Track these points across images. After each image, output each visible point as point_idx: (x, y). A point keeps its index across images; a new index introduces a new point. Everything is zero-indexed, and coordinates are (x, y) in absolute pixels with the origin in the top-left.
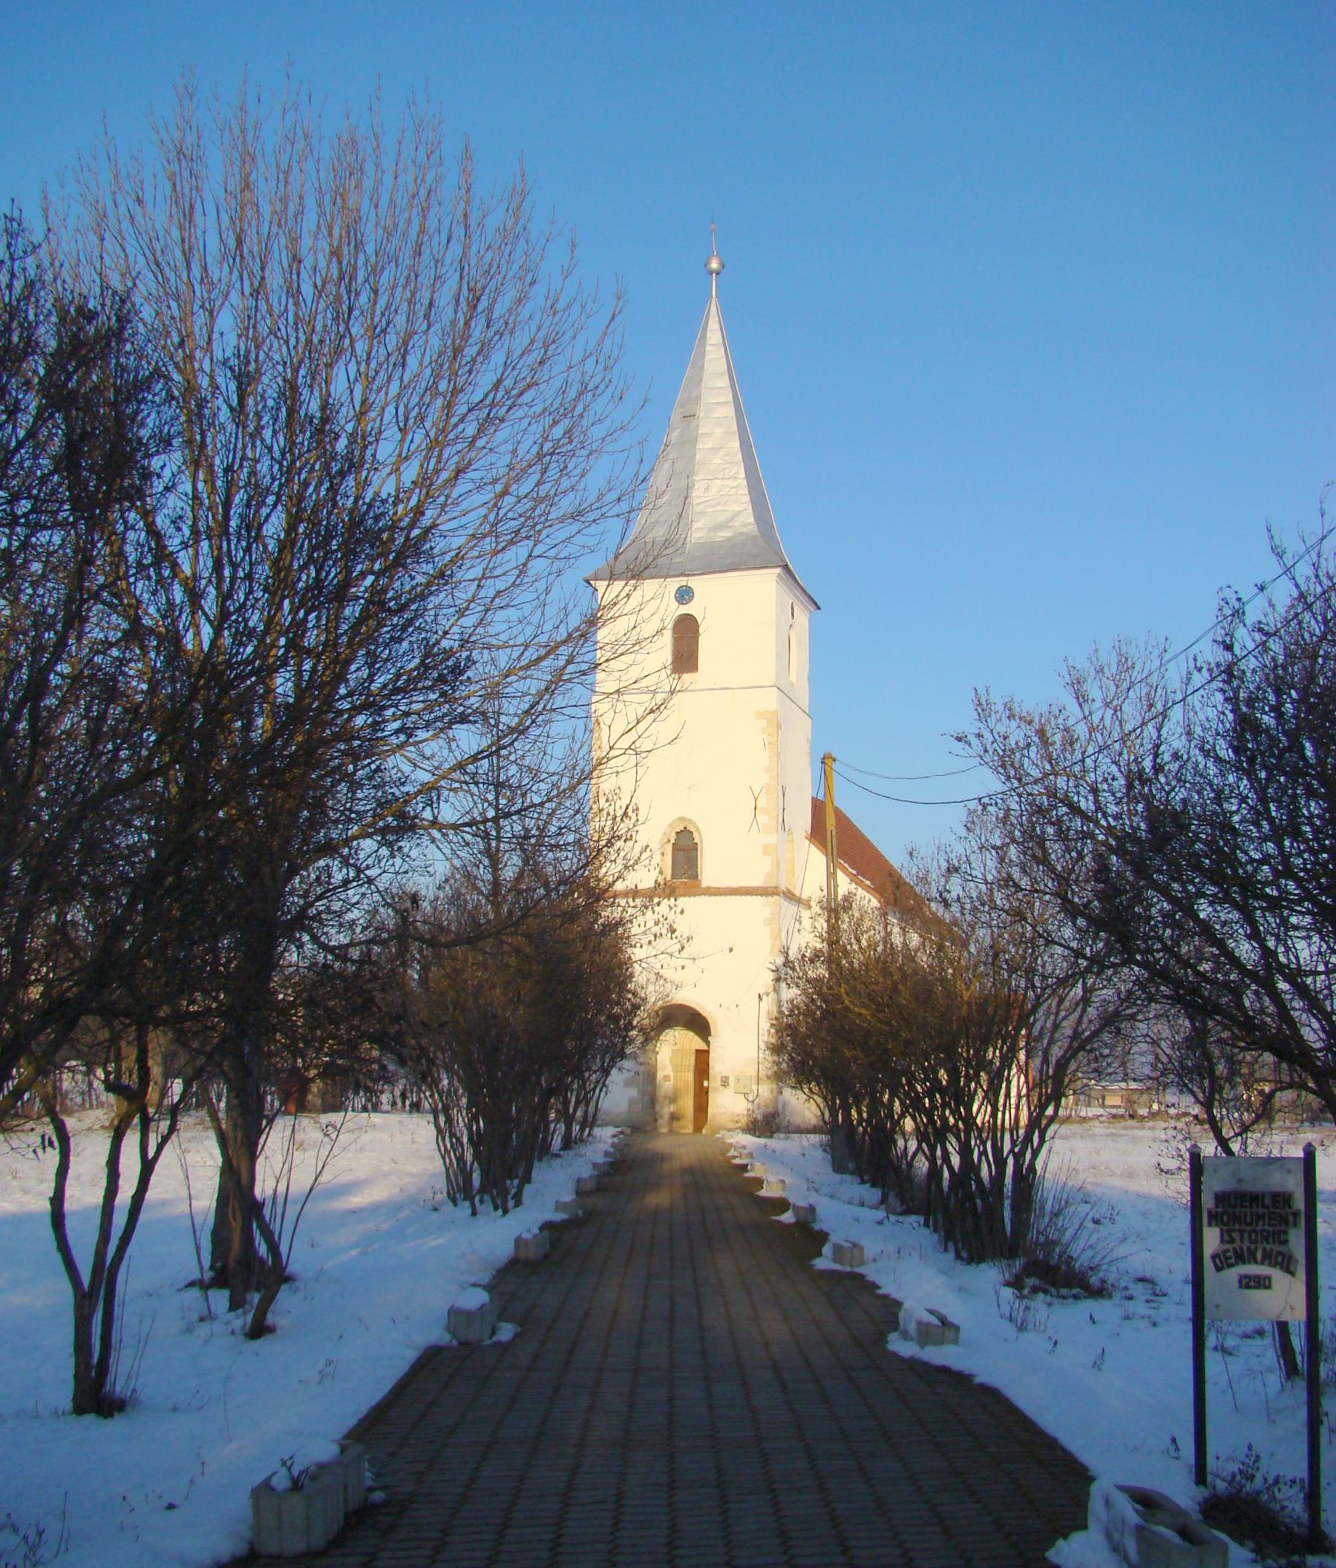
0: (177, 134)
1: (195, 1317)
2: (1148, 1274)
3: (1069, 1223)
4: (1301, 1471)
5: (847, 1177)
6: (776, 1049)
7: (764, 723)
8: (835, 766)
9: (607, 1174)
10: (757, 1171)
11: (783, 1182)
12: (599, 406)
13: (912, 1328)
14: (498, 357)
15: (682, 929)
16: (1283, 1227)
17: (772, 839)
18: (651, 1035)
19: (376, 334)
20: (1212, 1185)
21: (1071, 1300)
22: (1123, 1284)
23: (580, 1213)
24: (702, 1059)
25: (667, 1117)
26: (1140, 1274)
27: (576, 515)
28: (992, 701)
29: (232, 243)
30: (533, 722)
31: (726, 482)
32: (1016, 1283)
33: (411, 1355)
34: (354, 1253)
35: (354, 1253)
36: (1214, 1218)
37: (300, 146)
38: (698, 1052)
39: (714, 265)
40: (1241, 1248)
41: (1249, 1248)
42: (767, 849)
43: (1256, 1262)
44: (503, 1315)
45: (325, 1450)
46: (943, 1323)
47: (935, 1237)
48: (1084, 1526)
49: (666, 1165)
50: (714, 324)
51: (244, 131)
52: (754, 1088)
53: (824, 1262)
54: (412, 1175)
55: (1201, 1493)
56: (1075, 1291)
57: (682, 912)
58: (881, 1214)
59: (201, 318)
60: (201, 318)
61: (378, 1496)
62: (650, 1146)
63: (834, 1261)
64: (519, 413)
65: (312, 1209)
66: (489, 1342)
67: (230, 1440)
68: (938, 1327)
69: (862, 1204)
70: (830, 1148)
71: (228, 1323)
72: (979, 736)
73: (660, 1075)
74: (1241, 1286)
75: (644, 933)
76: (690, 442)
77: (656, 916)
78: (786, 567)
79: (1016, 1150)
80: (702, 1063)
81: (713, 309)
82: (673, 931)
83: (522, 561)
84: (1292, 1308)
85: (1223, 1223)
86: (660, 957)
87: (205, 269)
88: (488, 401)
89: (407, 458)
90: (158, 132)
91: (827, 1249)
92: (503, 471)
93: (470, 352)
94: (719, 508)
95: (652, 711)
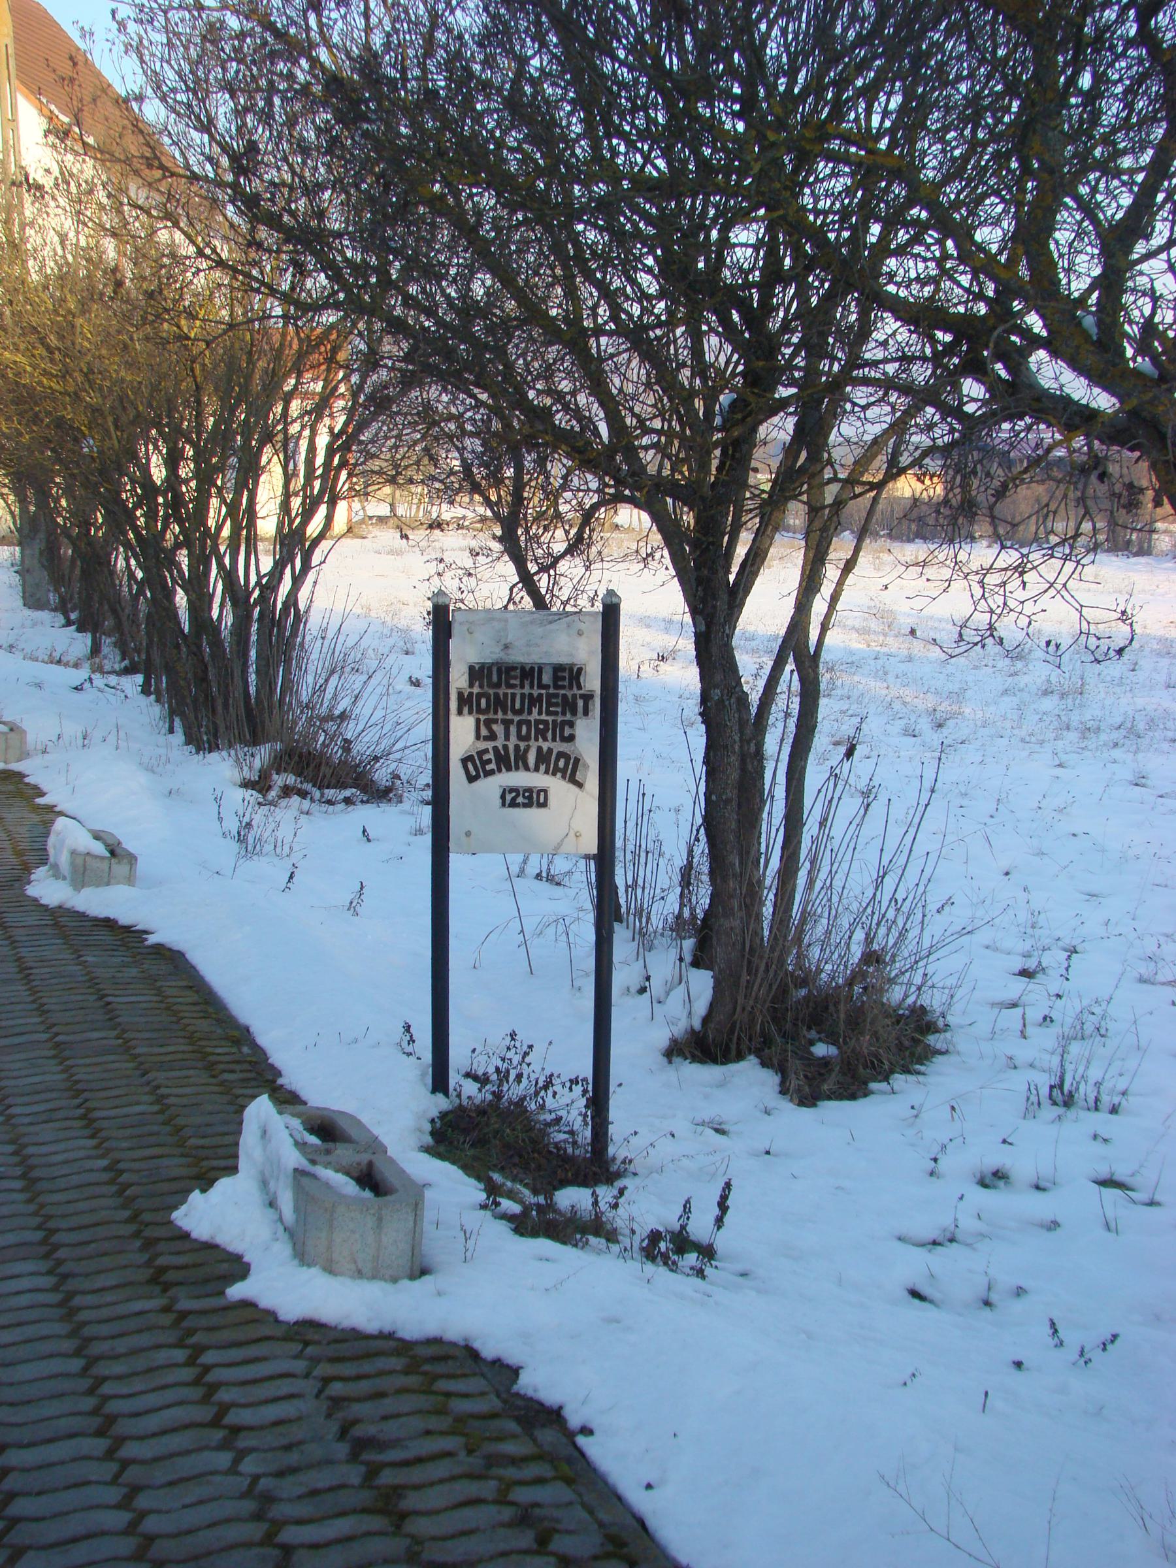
4: (585, 1068)
5: (45, 616)
13: (64, 860)
16: (568, 717)
21: (342, 806)
32: (260, 784)
36: (465, 701)
40: (505, 747)
41: (517, 747)
43: (527, 768)
46: (113, 853)
48: (233, 1170)
56: (348, 793)
68: (102, 858)
85: (480, 711)
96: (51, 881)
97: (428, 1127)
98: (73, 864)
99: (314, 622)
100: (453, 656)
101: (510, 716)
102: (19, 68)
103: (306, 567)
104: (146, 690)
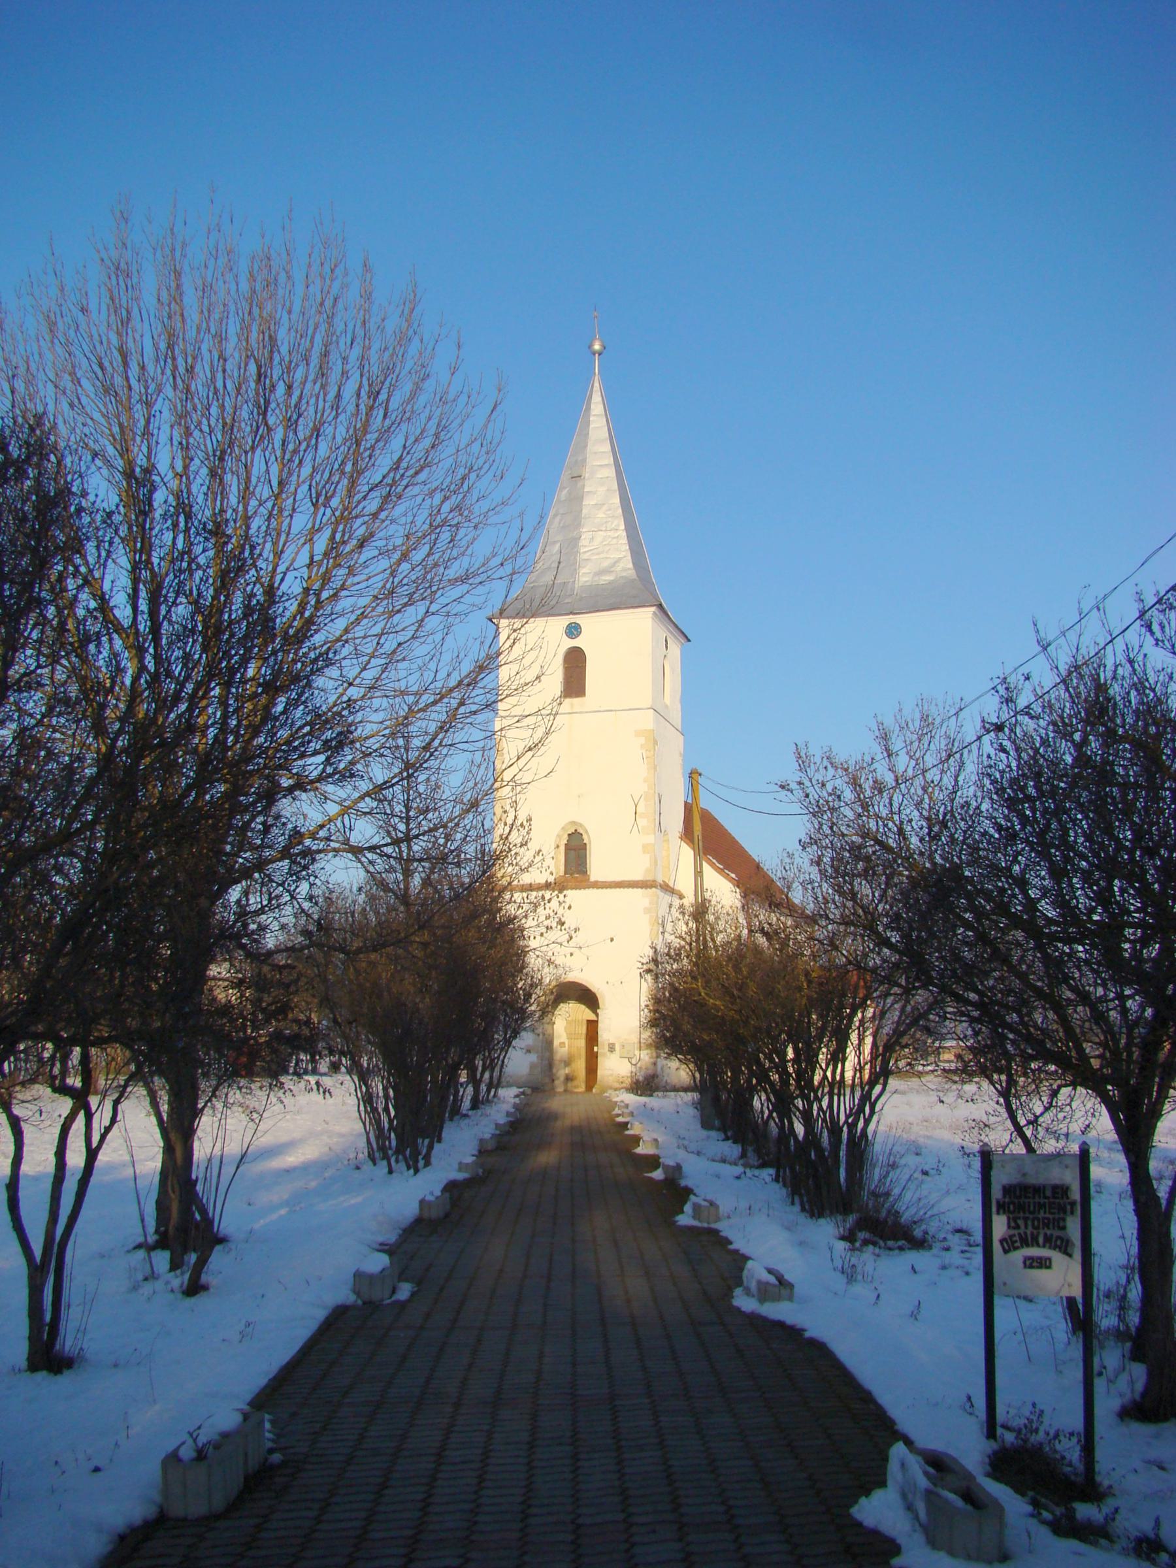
0: (114, 253)
1: (140, 1277)
2: (964, 1227)
3: (899, 1177)
4: (1078, 1424)
5: (713, 1134)
6: (653, 1023)
7: (642, 740)
8: (700, 780)
9: (508, 1133)
10: (635, 1129)
11: (656, 1140)
12: (482, 485)
13: (753, 1286)
14: (396, 443)
15: (570, 923)
16: (1062, 1215)
17: (651, 839)
18: (548, 1009)
19: (291, 424)
20: (1000, 1178)
21: (897, 1251)
22: (941, 1235)
23: (480, 1171)
24: (592, 1028)
25: (562, 1078)
26: (958, 1226)
27: (463, 579)
28: (811, 752)
29: (163, 346)
30: (431, 755)
31: (609, 533)
32: (849, 1237)
33: (321, 1314)
34: (283, 1212)
35: (283, 1212)
36: (1002, 1207)
37: (222, 260)
38: (589, 1022)
39: (597, 347)
41: (1032, 1234)
42: (646, 848)
43: (1038, 1245)
44: (402, 1277)
45: (227, 1418)
47: (784, 1191)
48: (882, 1484)
49: (559, 1124)
50: (597, 398)
51: (173, 250)
52: (637, 1053)
53: (685, 1219)
54: (342, 1135)
55: (991, 1446)
56: (900, 1243)
57: (570, 908)
58: (739, 1170)
59: (139, 412)
60: (139, 412)
61: (277, 1457)
62: (546, 1105)
63: (694, 1217)
64: (416, 490)
65: (252, 1169)
66: (388, 1301)
67: (155, 1401)
68: (774, 1286)
69: (724, 1161)
70: (699, 1105)
71: (167, 1283)
72: (800, 783)
73: (556, 1043)
74: (1025, 1266)
75: (538, 926)
76: (577, 499)
77: (548, 911)
78: (660, 606)
79: (850, 1120)
80: (592, 1031)
81: (596, 384)
82: (563, 924)
83: (419, 618)
84: (1069, 1285)
85: (1009, 1212)
86: (551, 946)
87: (143, 368)
88: (389, 480)
89: (319, 530)
90: (98, 252)
91: (688, 1208)
92: (399, 542)
93: (371, 437)
94: (602, 556)
95: (530, 749)
96: (745, 1297)
97: (987, 1460)
98: (759, 1290)
99: (877, 1148)
100: (993, 1179)
101: (1027, 1215)
102: (704, 847)
103: (872, 1112)
104: (777, 1180)
